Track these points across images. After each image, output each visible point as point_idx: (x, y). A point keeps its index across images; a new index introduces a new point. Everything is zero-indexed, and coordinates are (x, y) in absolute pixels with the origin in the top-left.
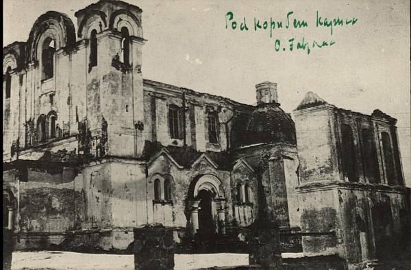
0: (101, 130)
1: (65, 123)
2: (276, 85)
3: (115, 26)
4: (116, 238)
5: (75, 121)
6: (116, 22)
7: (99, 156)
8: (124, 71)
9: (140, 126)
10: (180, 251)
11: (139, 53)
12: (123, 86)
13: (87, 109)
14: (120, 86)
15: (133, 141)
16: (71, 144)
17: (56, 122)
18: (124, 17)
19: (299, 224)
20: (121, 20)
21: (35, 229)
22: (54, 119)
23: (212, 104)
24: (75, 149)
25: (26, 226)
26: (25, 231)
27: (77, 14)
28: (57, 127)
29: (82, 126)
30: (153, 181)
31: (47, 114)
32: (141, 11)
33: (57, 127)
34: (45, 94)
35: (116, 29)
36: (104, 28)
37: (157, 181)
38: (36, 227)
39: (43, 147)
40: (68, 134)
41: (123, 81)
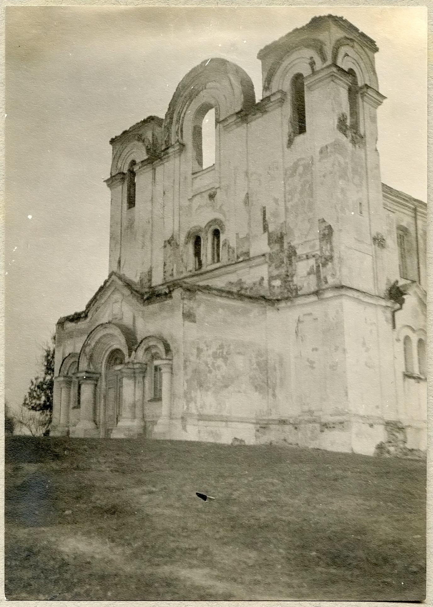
1: (241, 236)
4: (357, 435)
11: (374, 119)
13: (287, 209)
16: (252, 270)
17: (222, 237)
19: (216, 366)
24: (262, 279)
27: (264, 54)
29: (36, 371)
30: (402, 338)
31: (203, 225)
32: (376, 50)
33: (224, 245)
36: (319, 65)
37: (407, 338)
38: (211, 406)
40: (247, 253)
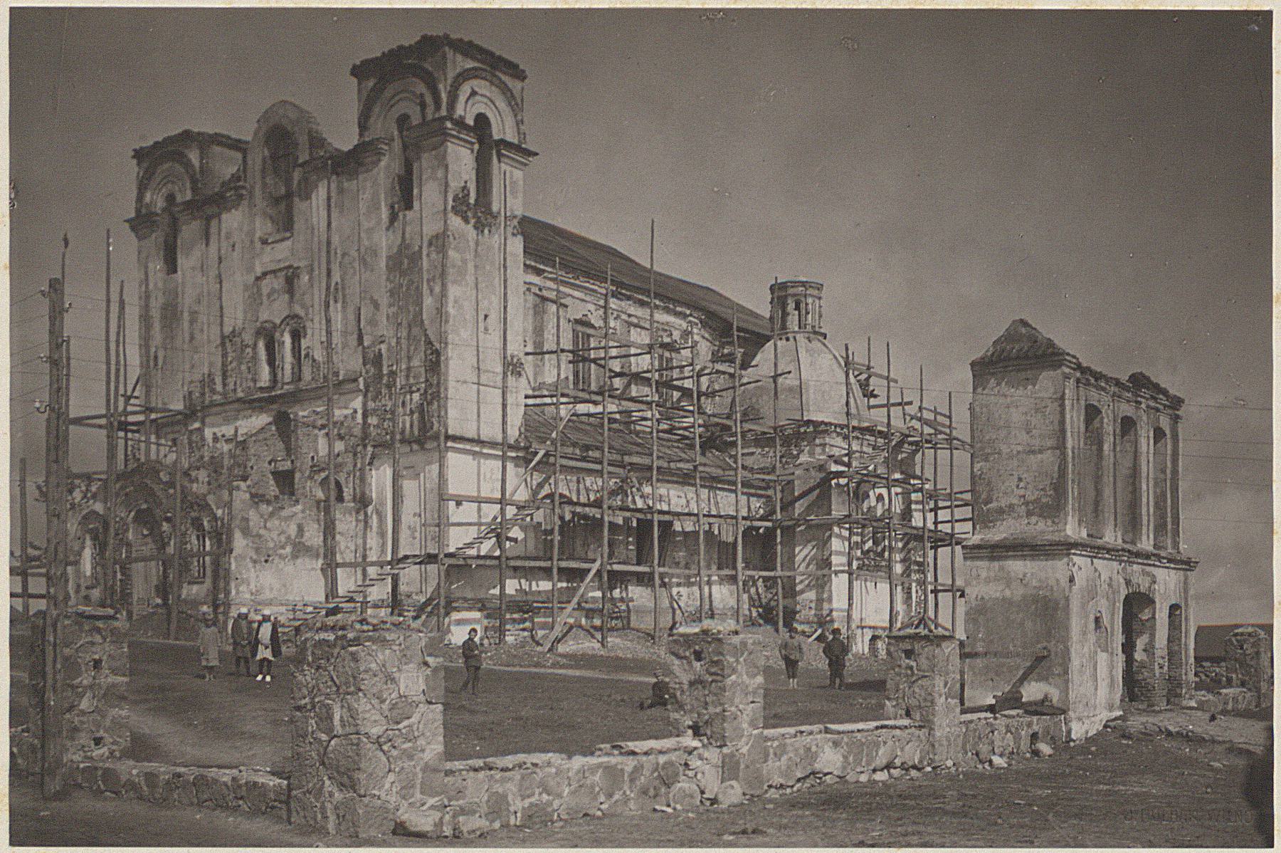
0: (423, 370)
2: (820, 287)
3: (459, 111)
5: (355, 343)
6: (462, 99)
7: (416, 433)
8: (479, 227)
9: (515, 365)
10: (121, 841)
12: (476, 267)
14: (471, 266)
15: (212, 418)
18: (481, 86)
20: (474, 93)
21: (267, 592)
22: (297, 336)
23: (667, 323)
24: (355, 411)
25: (249, 585)
26: (248, 596)
28: (307, 355)
31: (278, 321)
33: (307, 355)
34: (274, 272)
35: (462, 118)
39: (272, 400)
41: (476, 256)
